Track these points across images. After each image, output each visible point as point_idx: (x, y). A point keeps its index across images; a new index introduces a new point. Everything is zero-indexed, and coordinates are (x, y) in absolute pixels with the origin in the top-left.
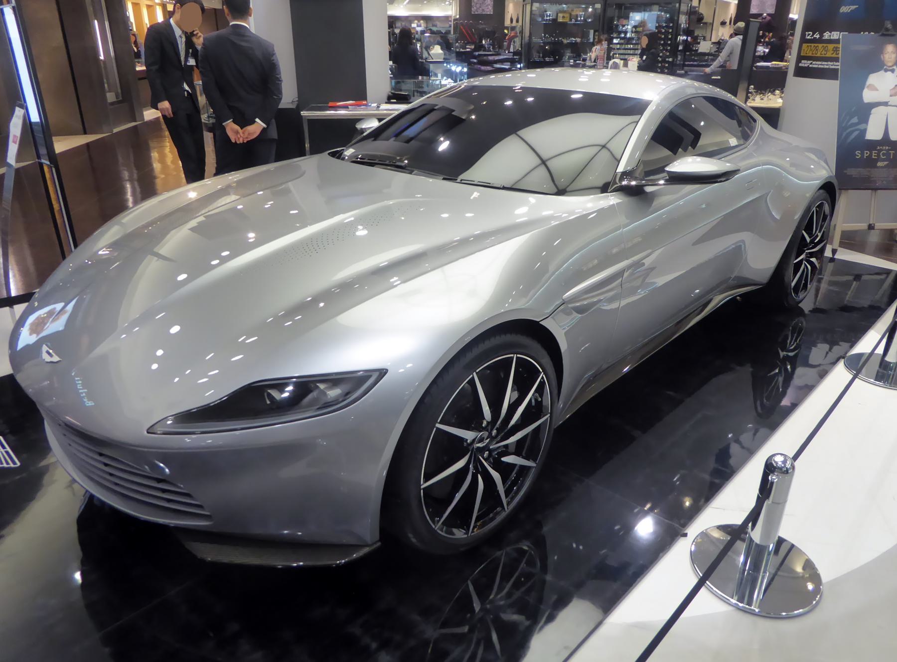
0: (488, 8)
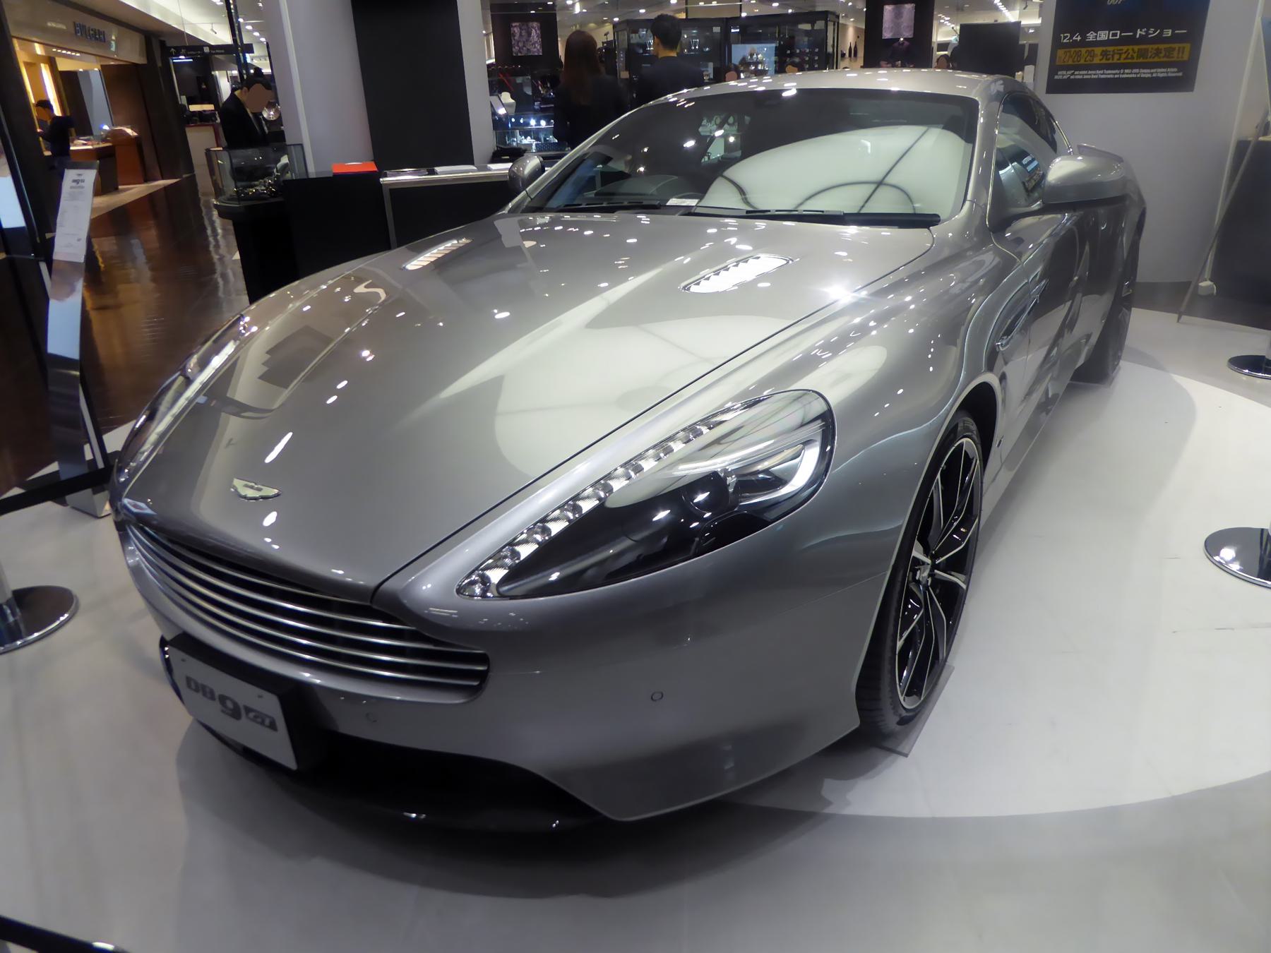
0: (535, 47)
